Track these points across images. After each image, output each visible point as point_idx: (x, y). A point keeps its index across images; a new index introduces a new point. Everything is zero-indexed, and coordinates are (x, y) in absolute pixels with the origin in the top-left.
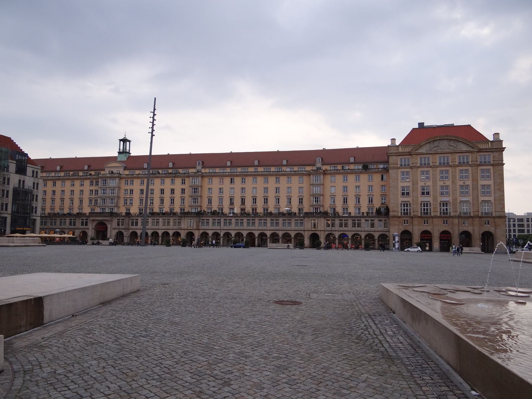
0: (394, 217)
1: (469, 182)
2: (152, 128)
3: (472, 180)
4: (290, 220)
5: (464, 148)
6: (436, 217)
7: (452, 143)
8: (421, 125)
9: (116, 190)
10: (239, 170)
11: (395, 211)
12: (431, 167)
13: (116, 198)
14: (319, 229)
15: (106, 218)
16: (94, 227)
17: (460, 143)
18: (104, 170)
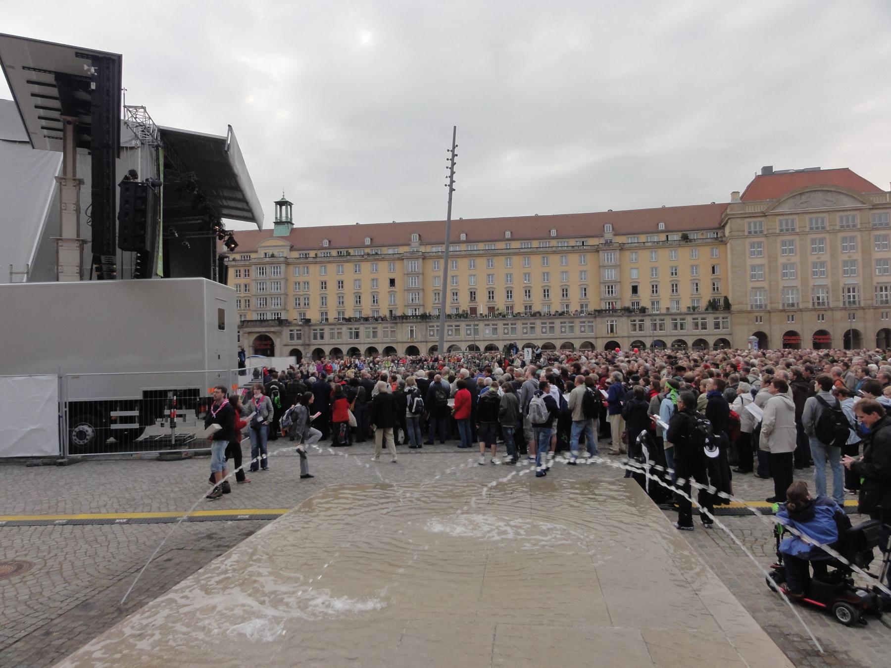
0: (741, 312)
1: (857, 256)
2: (451, 177)
3: (863, 252)
4: (572, 322)
5: (849, 203)
6: (807, 310)
7: (829, 196)
8: (767, 170)
9: (283, 283)
10: (481, 246)
11: (741, 303)
12: (798, 234)
13: (283, 297)
14: (620, 333)
15: (272, 329)
16: (251, 344)
17: (842, 196)
18: (256, 252)
